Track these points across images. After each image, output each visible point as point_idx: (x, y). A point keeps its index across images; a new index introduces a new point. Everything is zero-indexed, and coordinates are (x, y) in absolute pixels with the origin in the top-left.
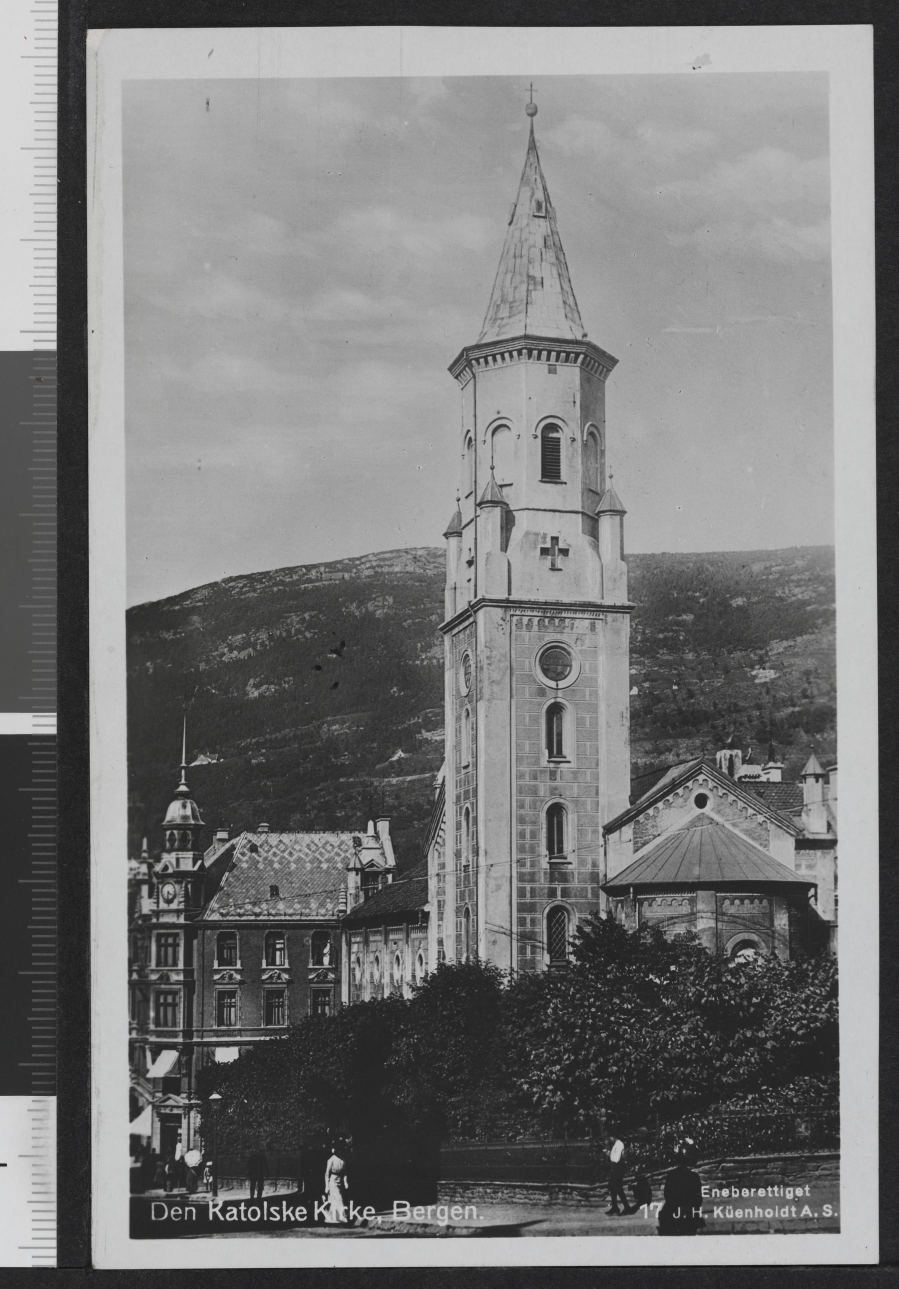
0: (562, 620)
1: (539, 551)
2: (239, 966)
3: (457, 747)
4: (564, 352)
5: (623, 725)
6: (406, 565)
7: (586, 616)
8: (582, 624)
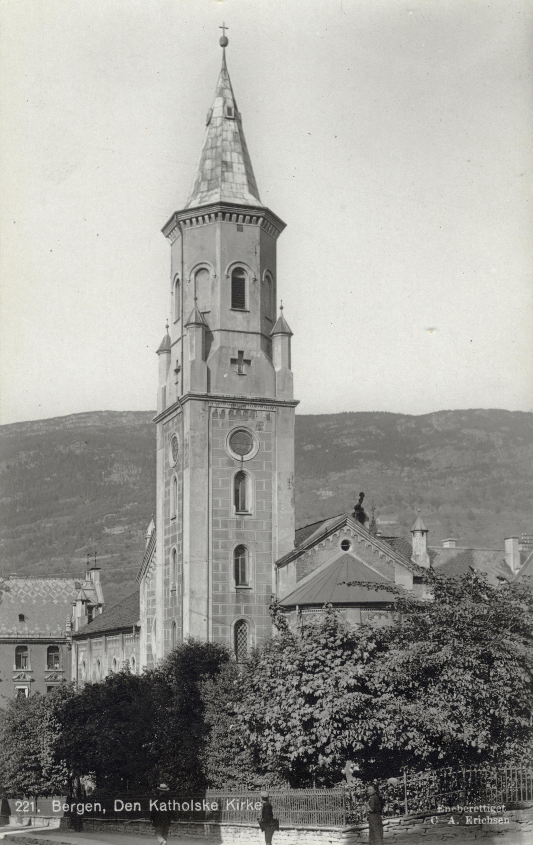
3: (166, 504)
4: (249, 215)
5: (290, 488)
6: (95, 422)
7: (263, 409)
8: (261, 414)
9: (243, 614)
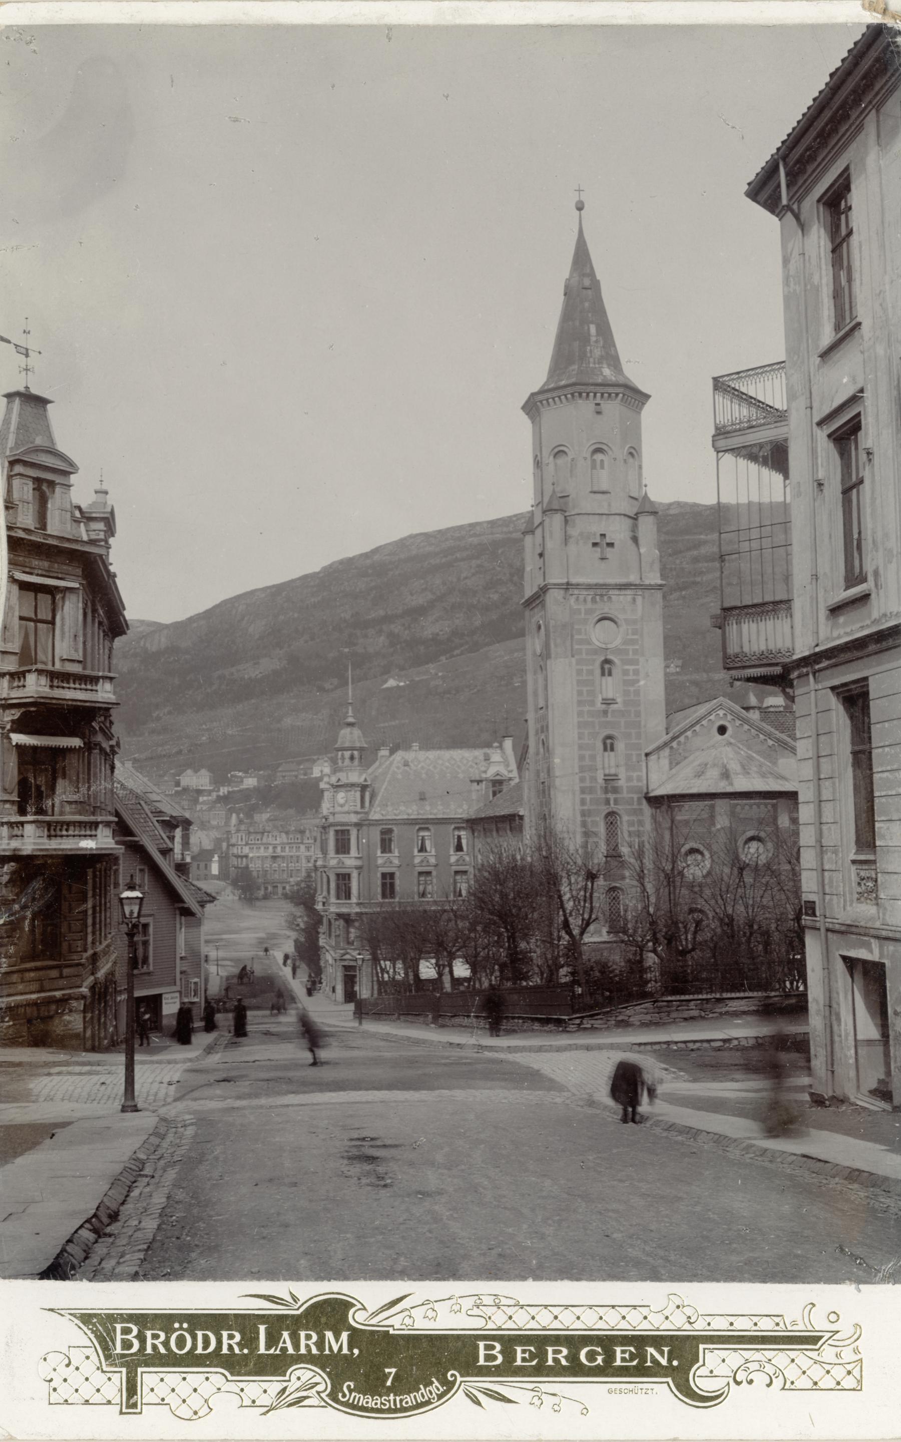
1: (591, 545)
2: (397, 854)
3: (535, 694)
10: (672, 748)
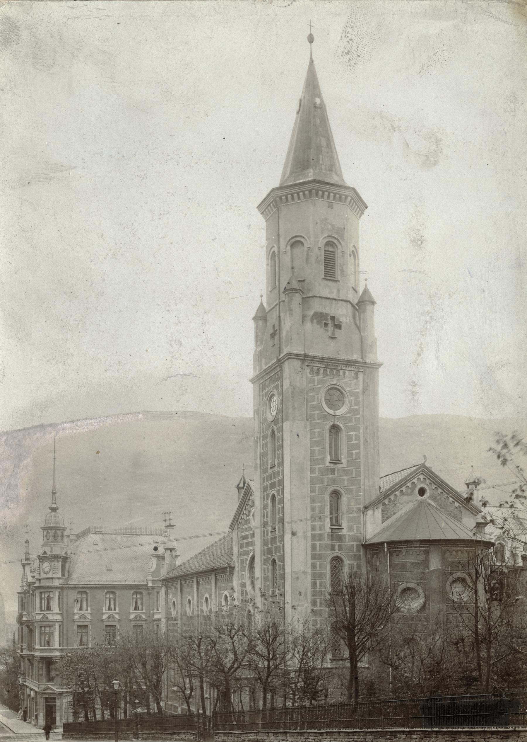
0: (338, 371)
9: (337, 551)
10: (384, 504)
